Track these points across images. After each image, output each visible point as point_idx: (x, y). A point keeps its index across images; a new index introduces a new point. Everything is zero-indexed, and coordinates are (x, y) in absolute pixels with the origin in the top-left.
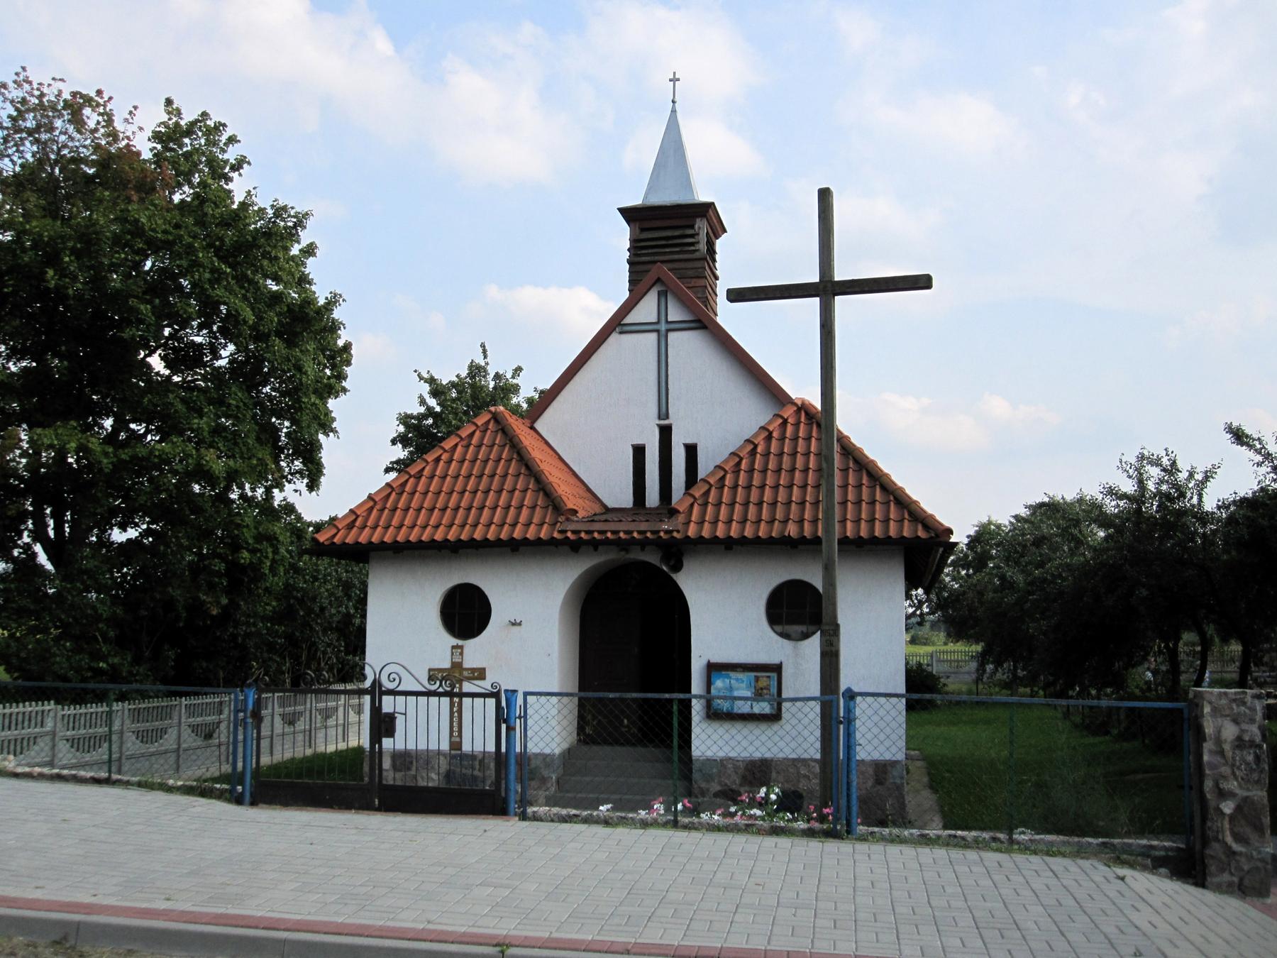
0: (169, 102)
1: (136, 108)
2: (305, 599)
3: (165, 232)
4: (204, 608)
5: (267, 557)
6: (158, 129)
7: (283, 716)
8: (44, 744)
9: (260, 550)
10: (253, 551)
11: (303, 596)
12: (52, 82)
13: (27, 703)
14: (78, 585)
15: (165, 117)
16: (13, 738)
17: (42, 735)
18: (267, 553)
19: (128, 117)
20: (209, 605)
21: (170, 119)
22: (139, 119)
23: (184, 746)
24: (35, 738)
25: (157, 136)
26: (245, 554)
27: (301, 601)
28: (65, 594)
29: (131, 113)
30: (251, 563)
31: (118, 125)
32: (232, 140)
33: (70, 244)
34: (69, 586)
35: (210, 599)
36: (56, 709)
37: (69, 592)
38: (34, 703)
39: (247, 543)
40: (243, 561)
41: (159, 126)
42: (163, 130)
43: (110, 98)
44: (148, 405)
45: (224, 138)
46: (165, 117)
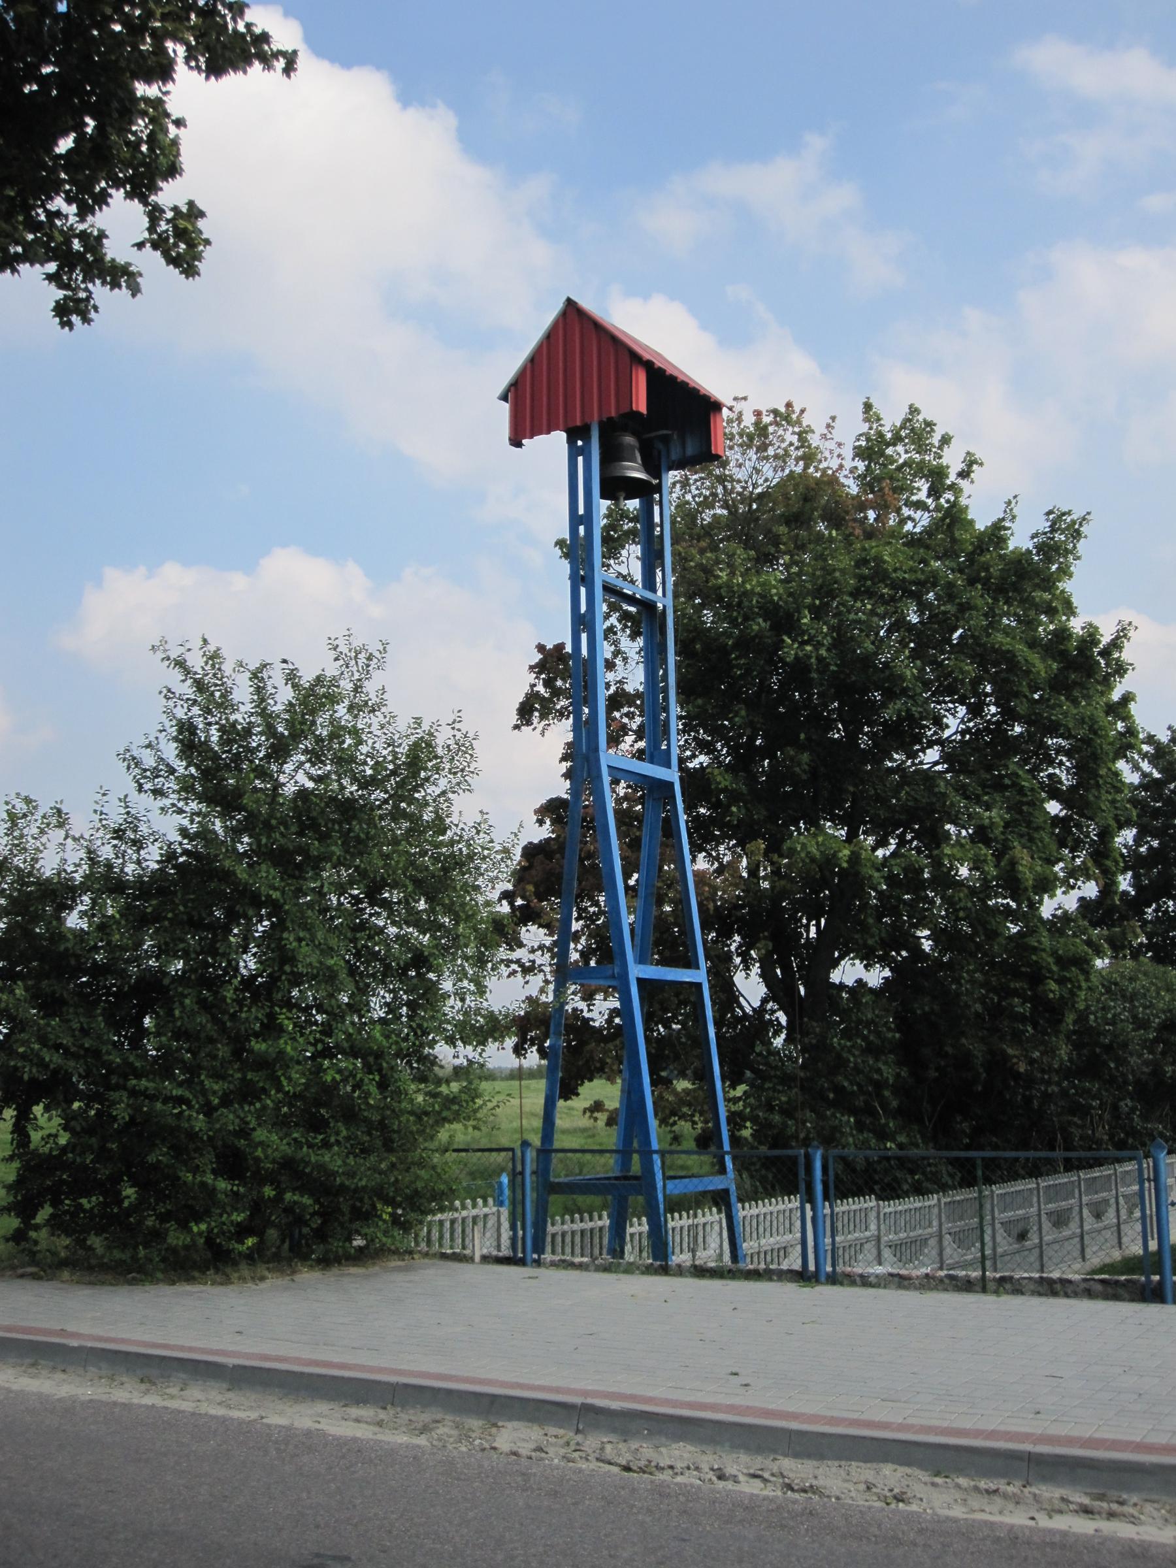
0: (868, 407)
1: (833, 418)
2: (1115, 1045)
3: (912, 570)
4: (1009, 1064)
5: (1080, 988)
6: (857, 444)
7: (1049, 1214)
8: (931, 1250)
9: (1070, 980)
10: (1061, 981)
11: (1111, 1042)
12: (734, 403)
13: (850, 1200)
14: (859, 1041)
15: (865, 427)
16: (769, 1248)
17: (868, 1240)
18: (1078, 981)
19: (825, 431)
20: (1015, 1060)
21: (871, 428)
22: (837, 435)
23: (1000, 1250)
24: (862, 1245)
25: (859, 453)
26: (1053, 986)
27: (1109, 1048)
28: (845, 1055)
29: (828, 426)
30: (1062, 997)
31: (814, 440)
32: (946, 440)
33: (808, 600)
34: (848, 1044)
35: (1017, 1053)
36: (878, 1205)
37: (850, 1052)
38: (850, 1200)
39: (1050, 971)
40: (1051, 996)
41: (858, 440)
42: (864, 444)
43: (803, 411)
44: (907, 800)
45: (936, 439)
46: (865, 427)
